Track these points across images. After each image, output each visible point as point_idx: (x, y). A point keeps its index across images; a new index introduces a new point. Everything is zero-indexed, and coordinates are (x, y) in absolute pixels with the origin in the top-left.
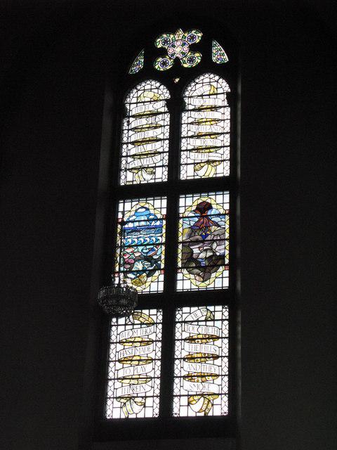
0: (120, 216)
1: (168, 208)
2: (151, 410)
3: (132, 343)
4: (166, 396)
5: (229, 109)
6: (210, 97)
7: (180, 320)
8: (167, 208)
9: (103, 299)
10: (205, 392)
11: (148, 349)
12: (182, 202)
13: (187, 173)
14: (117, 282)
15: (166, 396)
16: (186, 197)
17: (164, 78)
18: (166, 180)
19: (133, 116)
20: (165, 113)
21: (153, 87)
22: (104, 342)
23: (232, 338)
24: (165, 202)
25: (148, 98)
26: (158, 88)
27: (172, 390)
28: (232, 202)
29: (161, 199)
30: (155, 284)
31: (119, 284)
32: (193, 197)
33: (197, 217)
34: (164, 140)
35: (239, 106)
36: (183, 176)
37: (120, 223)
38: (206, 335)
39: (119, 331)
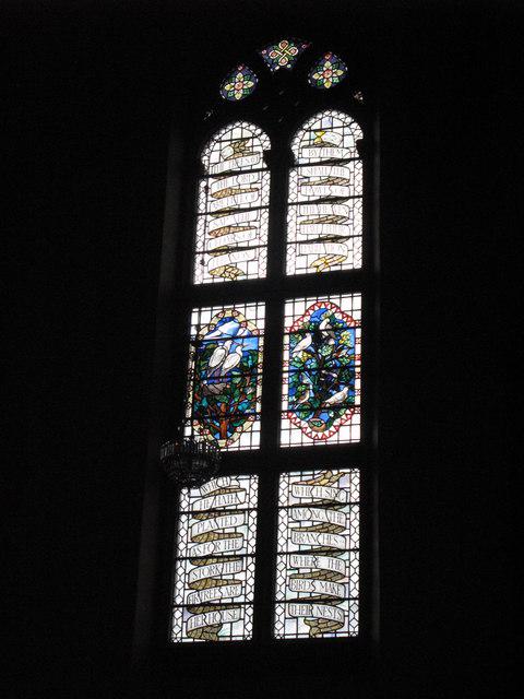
0: (193, 331)
3: (213, 523)
6: (332, 142)
7: (285, 505)
9: (169, 458)
11: (253, 197)
13: (296, 265)
19: (214, 176)
20: (262, 170)
22: (171, 515)
24: (262, 311)
25: (233, 159)
30: (248, 438)
31: (192, 436)
34: (249, 510)
35: (377, 160)
36: (290, 271)
37: (194, 344)
38: (325, 523)
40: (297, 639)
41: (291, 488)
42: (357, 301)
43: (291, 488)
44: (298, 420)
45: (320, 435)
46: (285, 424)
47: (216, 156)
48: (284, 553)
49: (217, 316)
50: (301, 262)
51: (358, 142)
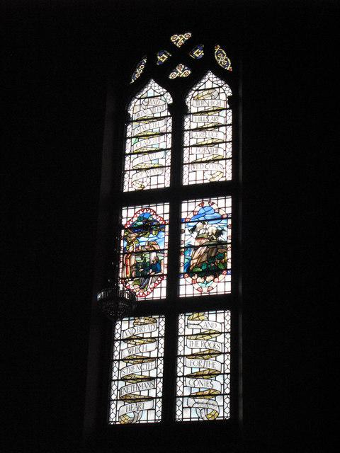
3: (136, 342)
4: (169, 398)
6: (212, 98)
8: (170, 213)
10: (207, 396)
12: (184, 206)
14: (121, 289)
15: (169, 398)
16: (188, 202)
18: (230, 179)
20: (167, 116)
22: (108, 341)
24: (167, 208)
25: (151, 104)
28: (234, 206)
30: (159, 292)
32: (195, 202)
33: (202, 246)
36: (185, 183)
38: (209, 337)
39: (119, 406)
40: (190, 421)
41: (186, 324)
42: (229, 201)
43: (186, 324)
44: (158, 220)
45: (145, 211)
46: (167, 217)
47: (136, 109)
48: (182, 356)
49: (213, 288)
50: (192, 176)
51: (229, 97)
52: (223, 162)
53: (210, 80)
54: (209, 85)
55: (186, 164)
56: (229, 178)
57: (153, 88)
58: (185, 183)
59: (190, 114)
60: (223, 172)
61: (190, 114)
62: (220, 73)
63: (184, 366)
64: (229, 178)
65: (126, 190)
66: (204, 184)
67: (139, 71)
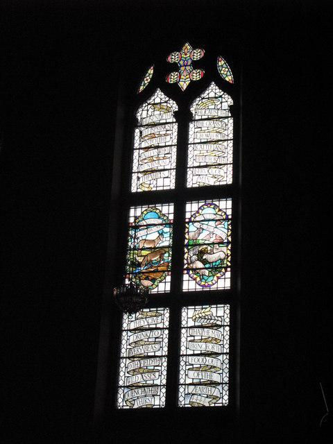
1: (175, 213)
2: (159, 401)
3: (142, 334)
5: (231, 121)
6: (215, 116)
10: (207, 381)
12: (188, 207)
17: (172, 91)
18: (174, 188)
20: (173, 123)
21: (162, 101)
23: (232, 325)
24: (172, 208)
25: (156, 113)
26: (166, 102)
27: (180, 322)
29: (169, 205)
30: (164, 287)
36: (189, 185)
38: (208, 338)
47: (145, 114)
48: (184, 355)
51: (230, 106)
52: (196, 141)
53: (213, 90)
54: (212, 95)
55: (136, 149)
56: (230, 181)
57: (159, 96)
58: (189, 185)
59: (195, 120)
60: (225, 176)
61: (195, 120)
62: (223, 85)
63: (187, 348)
64: (230, 181)
65: (134, 190)
66: (163, 191)
67: (147, 80)
